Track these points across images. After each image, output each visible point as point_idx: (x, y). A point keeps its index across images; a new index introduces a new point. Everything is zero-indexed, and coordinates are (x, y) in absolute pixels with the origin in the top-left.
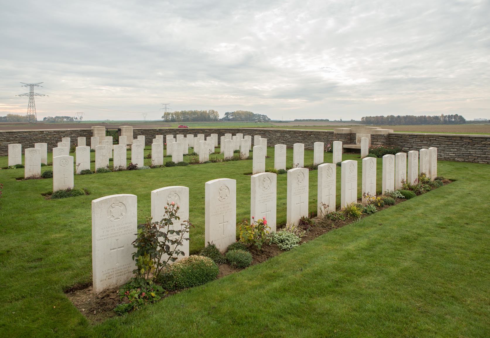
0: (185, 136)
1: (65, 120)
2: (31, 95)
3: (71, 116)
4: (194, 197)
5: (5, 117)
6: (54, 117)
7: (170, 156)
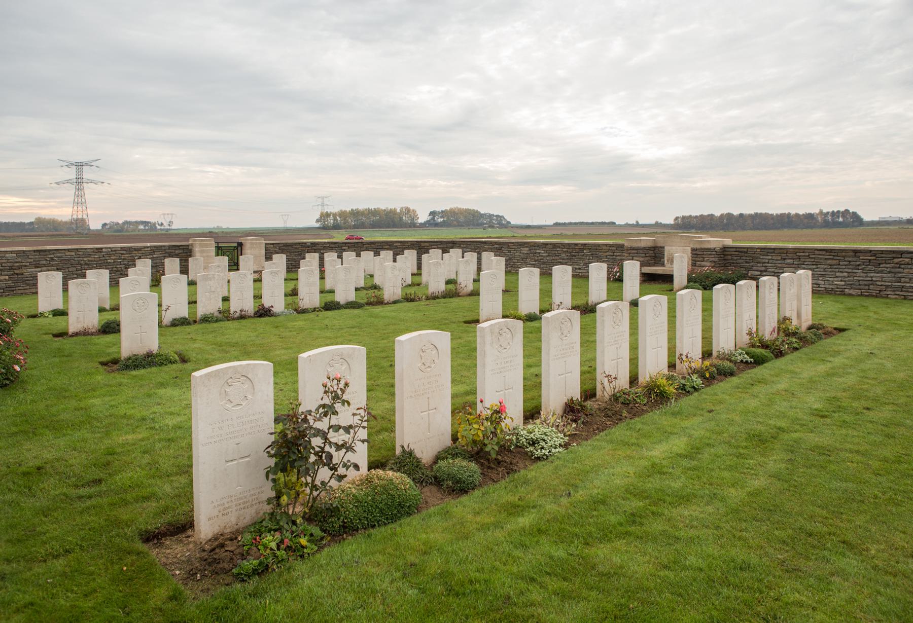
0: (358, 255)
1: (142, 227)
2: (79, 182)
3: (153, 221)
4: (375, 365)
5: (31, 223)
6: (120, 222)
7: (332, 292)
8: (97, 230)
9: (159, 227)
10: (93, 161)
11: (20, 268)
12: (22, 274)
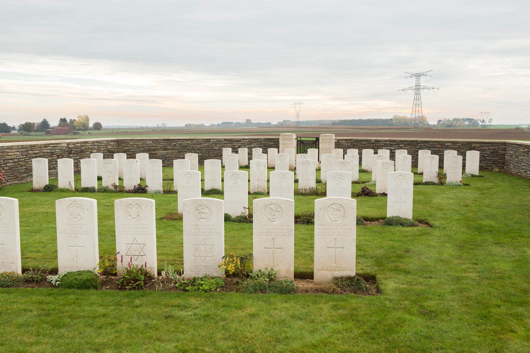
0: (376, 153)
2: (418, 88)
3: (475, 118)
5: (391, 119)
6: (451, 119)
8: (434, 126)
9: (481, 124)
10: (428, 72)
11: (154, 150)
12: (156, 154)
